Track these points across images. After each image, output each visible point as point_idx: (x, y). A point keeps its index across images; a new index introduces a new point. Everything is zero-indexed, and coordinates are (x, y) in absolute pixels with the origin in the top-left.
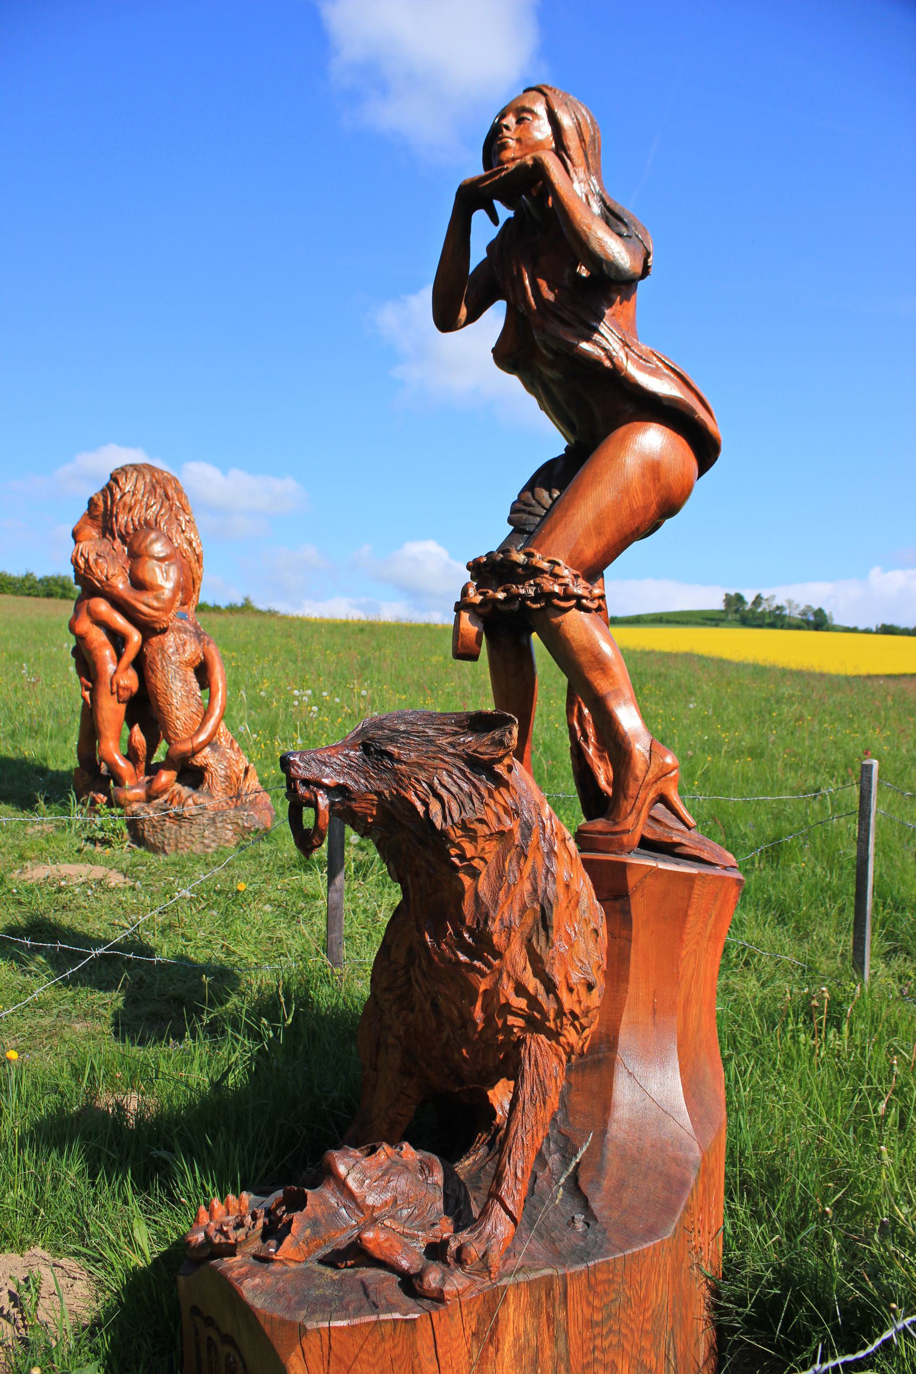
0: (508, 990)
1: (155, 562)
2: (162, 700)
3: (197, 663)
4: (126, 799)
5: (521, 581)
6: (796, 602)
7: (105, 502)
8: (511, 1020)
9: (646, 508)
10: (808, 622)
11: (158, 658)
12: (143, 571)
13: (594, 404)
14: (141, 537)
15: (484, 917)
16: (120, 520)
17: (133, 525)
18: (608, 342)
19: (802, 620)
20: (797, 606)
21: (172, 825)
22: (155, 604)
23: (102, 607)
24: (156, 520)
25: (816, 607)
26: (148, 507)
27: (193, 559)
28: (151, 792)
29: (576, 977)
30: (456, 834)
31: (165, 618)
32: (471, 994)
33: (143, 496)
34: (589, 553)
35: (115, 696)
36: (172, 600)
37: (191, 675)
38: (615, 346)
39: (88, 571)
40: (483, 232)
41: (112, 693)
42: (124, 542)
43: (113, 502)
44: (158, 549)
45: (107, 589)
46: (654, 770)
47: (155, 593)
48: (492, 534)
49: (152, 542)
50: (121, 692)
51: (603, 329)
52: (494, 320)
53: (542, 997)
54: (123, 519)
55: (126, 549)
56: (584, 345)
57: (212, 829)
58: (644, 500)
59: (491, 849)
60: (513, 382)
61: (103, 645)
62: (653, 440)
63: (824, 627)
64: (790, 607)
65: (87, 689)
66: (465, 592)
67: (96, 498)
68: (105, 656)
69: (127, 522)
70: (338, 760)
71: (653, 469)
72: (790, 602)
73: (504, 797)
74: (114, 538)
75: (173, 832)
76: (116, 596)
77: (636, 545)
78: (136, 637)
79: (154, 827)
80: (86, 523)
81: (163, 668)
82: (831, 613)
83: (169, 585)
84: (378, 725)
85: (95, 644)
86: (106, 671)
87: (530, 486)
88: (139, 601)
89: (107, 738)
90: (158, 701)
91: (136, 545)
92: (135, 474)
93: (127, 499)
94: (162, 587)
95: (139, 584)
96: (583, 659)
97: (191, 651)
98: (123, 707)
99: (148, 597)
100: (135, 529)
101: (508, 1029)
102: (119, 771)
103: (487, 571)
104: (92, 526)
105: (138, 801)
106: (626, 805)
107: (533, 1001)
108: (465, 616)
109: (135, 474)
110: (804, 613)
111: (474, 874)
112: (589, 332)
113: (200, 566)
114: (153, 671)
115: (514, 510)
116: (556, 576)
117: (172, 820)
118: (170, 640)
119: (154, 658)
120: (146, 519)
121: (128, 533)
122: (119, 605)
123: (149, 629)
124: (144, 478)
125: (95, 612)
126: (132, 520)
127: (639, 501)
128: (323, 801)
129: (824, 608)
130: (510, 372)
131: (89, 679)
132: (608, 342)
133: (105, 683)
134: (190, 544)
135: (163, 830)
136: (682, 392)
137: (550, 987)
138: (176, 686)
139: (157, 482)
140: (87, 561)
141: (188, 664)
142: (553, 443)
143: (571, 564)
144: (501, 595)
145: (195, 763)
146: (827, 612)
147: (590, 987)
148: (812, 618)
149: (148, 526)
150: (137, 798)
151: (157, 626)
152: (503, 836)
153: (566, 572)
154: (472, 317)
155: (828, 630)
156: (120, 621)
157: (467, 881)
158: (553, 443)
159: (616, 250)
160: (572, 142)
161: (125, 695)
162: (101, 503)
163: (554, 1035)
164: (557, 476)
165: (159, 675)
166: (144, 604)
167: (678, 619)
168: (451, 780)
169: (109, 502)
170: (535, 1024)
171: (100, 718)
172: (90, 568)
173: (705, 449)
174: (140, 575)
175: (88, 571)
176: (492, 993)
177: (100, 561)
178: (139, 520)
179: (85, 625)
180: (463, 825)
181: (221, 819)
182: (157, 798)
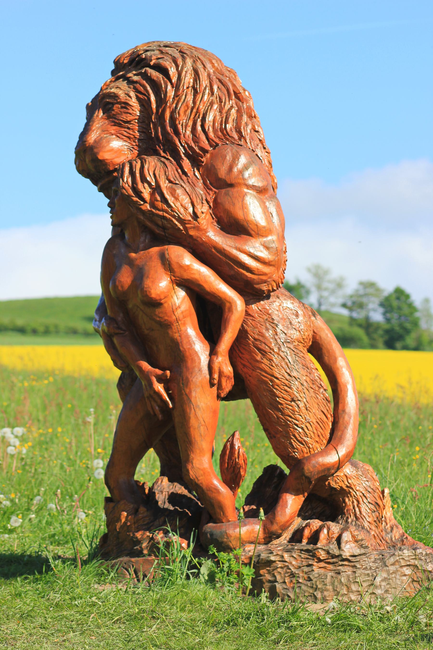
4: (239, 538)
6: (335, 274)
7: (144, 104)
10: (368, 326)
11: (269, 334)
19: (352, 321)
20: (340, 285)
21: (322, 571)
22: (263, 254)
23: (188, 260)
25: (388, 286)
28: (275, 528)
31: (275, 276)
35: (215, 388)
39: (160, 204)
41: (212, 385)
44: (252, 177)
45: (192, 233)
49: (246, 167)
57: (385, 575)
63: (410, 340)
64: (319, 288)
68: (188, 337)
72: (319, 274)
75: (329, 579)
76: (203, 244)
77: (82, 130)
79: (293, 575)
81: (279, 349)
82: (427, 301)
85: (178, 313)
89: (202, 451)
95: (236, 227)
99: (256, 247)
102: (221, 498)
110: (355, 304)
117: (322, 564)
118: (281, 306)
119: (261, 334)
120: (223, 130)
121: (205, 151)
122: (204, 254)
123: (252, 292)
129: (408, 288)
133: (200, 370)
135: (310, 580)
138: (298, 372)
145: (333, 484)
146: (417, 299)
148: (377, 316)
151: (264, 287)
155: (418, 347)
162: (134, 102)
166: (250, 252)
167: (20, 322)
171: (193, 422)
172: (165, 200)
175: (160, 204)
181: (392, 560)
182: (279, 536)
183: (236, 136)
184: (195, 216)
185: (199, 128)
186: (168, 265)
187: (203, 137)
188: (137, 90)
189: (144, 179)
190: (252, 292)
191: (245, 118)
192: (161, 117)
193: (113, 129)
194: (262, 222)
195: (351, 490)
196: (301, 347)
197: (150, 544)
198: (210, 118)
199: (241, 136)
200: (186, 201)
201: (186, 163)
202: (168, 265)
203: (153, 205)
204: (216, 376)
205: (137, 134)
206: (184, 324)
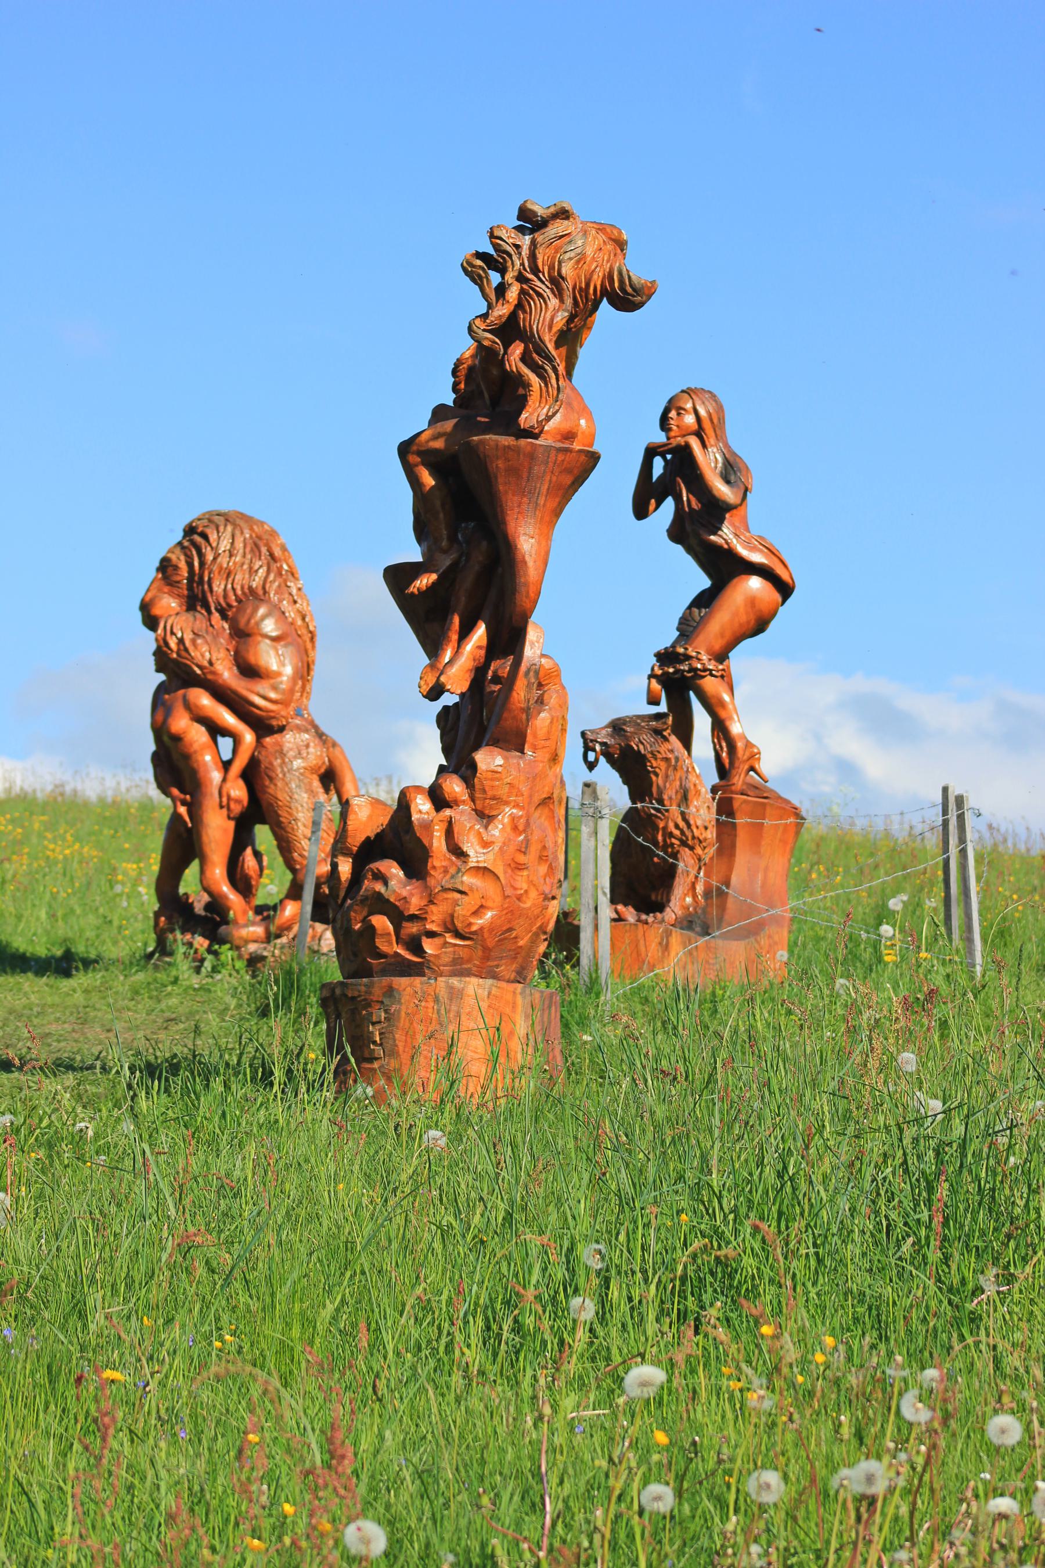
0: (671, 825)
1: (268, 641)
2: (285, 814)
3: (322, 770)
4: (241, 938)
5: (681, 662)
7: (190, 565)
8: (674, 841)
9: (748, 622)
12: (256, 654)
13: (723, 567)
14: (249, 611)
15: (660, 792)
16: (215, 588)
17: (235, 594)
18: (727, 535)
22: (273, 695)
23: (205, 701)
24: (264, 588)
26: (252, 572)
27: (307, 637)
29: (699, 823)
30: (649, 756)
31: (283, 713)
32: (656, 828)
33: (244, 556)
34: (718, 645)
35: (225, 811)
36: (292, 691)
37: (316, 784)
38: (731, 537)
39: (183, 653)
40: (658, 466)
41: (221, 807)
42: (224, 617)
43: (202, 564)
44: (269, 626)
45: (210, 677)
46: (747, 754)
47: (272, 681)
48: (667, 637)
50: (232, 805)
51: (725, 530)
52: (666, 512)
53: (685, 829)
54: (218, 587)
55: (226, 626)
56: (712, 537)
58: (745, 618)
59: (663, 765)
60: (679, 549)
61: (204, 747)
62: (755, 583)
65: (184, 803)
66: (653, 669)
67: (173, 557)
68: (205, 764)
69: (225, 590)
70: (604, 732)
71: (752, 601)
73: (667, 746)
74: (209, 612)
78: (249, 737)
80: (160, 590)
83: (288, 670)
84: (619, 719)
85: (196, 746)
86: (211, 781)
87: (689, 607)
88: (253, 692)
90: (279, 816)
91: (242, 621)
92: (229, 528)
93: (223, 560)
94: (279, 674)
95: (250, 671)
96: (713, 701)
97: (315, 754)
98: (232, 824)
100: (239, 601)
101: (672, 844)
103: (665, 657)
104: (171, 594)
105: (255, 941)
106: (734, 772)
107: (682, 832)
108: (654, 681)
109: (229, 528)
111: (657, 775)
112: (716, 530)
113: (314, 647)
114: (271, 779)
115: (680, 623)
116: (699, 660)
118: (290, 739)
119: (271, 764)
120: (250, 588)
121: (230, 606)
123: (263, 726)
124: (242, 533)
125: (197, 706)
126: (233, 589)
127: (743, 618)
128: (598, 747)
130: (625, 783)
131: (183, 791)
132: (727, 535)
133: (212, 795)
134: (303, 619)
136: (767, 557)
137: (689, 826)
138: (302, 797)
139: (259, 537)
140: (181, 641)
141: (313, 770)
142: (706, 583)
143: (708, 652)
144: (671, 670)
147: (706, 828)
149: (255, 596)
150: (254, 937)
151: (274, 723)
152: (667, 760)
153: (704, 657)
154: (658, 505)
156: (229, 719)
157: (654, 778)
158: (706, 583)
159: (723, 490)
160: (707, 425)
161: (236, 809)
162: (183, 565)
163: (692, 848)
164: (705, 600)
165: (280, 784)
166: (260, 696)
168: (647, 738)
169: (196, 564)
170: (684, 843)
171: (205, 839)
172: (186, 650)
173: (785, 589)
174: (252, 659)
175: (183, 653)
176: (665, 828)
177: (199, 641)
178: (242, 588)
179: (181, 723)
180: (652, 753)
183: (260, 592)
184: (211, 663)
185: (229, 586)
186: (188, 706)
187: (231, 594)
188: (186, 555)
189: (173, 633)
190: (263, 726)
191: (272, 577)
192: (201, 577)
193: (166, 589)
194: (274, 667)
195: (239, 592)
196: (308, 774)
197: (654, 790)
198: (239, 577)
199: (265, 592)
200: (205, 648)
201: (216, 616)
202: (188, 706)
203: (178, 655)
204: (225, 800)
205: (186, 592)
206: (203, 755)
